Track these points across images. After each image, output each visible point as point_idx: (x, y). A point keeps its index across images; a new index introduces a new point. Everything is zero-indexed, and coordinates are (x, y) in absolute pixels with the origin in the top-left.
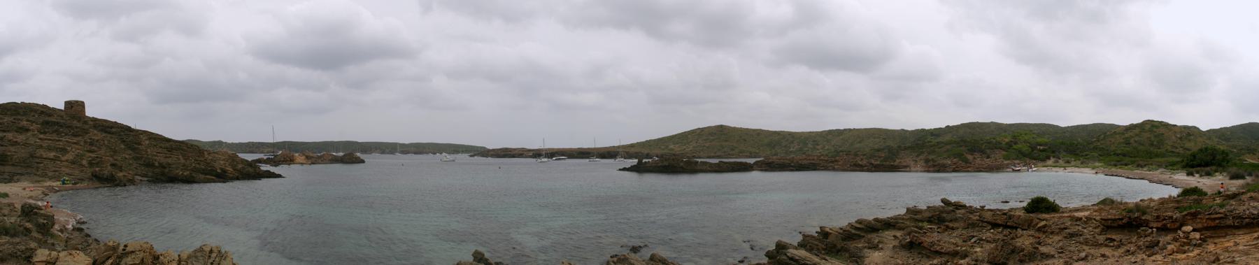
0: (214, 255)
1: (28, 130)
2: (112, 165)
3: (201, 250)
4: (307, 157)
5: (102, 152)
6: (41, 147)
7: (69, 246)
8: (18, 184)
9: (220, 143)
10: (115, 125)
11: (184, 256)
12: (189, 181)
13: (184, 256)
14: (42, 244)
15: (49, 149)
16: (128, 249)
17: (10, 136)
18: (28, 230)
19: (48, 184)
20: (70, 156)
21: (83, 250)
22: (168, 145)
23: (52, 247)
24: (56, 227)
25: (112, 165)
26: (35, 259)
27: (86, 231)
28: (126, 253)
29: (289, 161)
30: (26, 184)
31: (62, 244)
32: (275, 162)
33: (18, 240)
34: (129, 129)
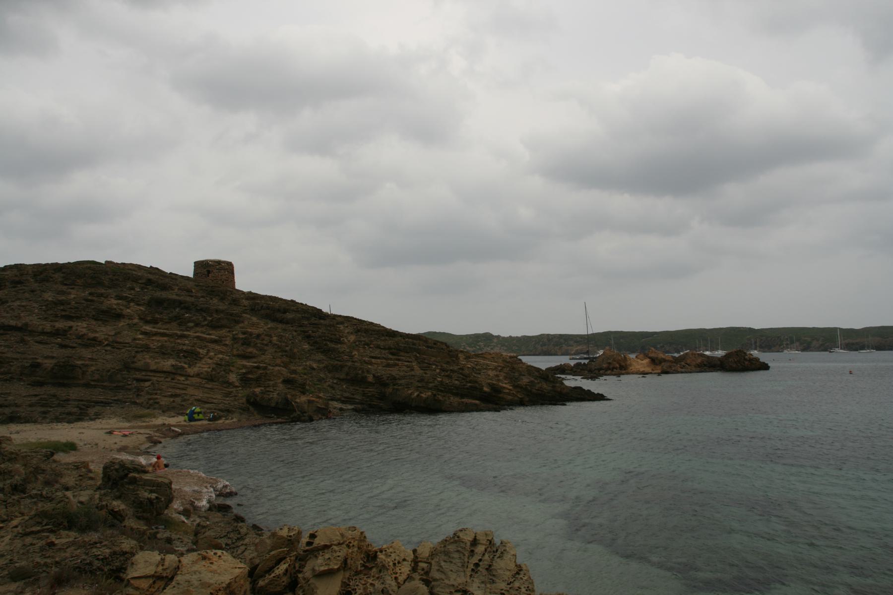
0: (480, 549)
1: (119, 316)
2: (287, 381)
3: (456, 539)
4: (654, 361)
5: (267, 357)
6: (146, 348)
7: (200, 541)
8: (97, 424)
9: (487, 338)
10: (292, 306)
11: (424, 552)
12: (431, 408)
13: (424, 552)
14: (146, 541)
15: (163, 352)
16: (318, 542)
17: (81, 327)
18: (117, 516)
19: (159, 421)
20: (203, 367)
21: (229, 548)
22: (390, 342)
23: (167, 546)
24: (177, 505)
25: (287, 381)
26: (131, 573)
27: (236, 511)
28: (313, 551)
29: (619, 368)
30: (113, 422)
31: (188, 539)
32: (592, 371)
33: (94, 536)
34: (317, 314)
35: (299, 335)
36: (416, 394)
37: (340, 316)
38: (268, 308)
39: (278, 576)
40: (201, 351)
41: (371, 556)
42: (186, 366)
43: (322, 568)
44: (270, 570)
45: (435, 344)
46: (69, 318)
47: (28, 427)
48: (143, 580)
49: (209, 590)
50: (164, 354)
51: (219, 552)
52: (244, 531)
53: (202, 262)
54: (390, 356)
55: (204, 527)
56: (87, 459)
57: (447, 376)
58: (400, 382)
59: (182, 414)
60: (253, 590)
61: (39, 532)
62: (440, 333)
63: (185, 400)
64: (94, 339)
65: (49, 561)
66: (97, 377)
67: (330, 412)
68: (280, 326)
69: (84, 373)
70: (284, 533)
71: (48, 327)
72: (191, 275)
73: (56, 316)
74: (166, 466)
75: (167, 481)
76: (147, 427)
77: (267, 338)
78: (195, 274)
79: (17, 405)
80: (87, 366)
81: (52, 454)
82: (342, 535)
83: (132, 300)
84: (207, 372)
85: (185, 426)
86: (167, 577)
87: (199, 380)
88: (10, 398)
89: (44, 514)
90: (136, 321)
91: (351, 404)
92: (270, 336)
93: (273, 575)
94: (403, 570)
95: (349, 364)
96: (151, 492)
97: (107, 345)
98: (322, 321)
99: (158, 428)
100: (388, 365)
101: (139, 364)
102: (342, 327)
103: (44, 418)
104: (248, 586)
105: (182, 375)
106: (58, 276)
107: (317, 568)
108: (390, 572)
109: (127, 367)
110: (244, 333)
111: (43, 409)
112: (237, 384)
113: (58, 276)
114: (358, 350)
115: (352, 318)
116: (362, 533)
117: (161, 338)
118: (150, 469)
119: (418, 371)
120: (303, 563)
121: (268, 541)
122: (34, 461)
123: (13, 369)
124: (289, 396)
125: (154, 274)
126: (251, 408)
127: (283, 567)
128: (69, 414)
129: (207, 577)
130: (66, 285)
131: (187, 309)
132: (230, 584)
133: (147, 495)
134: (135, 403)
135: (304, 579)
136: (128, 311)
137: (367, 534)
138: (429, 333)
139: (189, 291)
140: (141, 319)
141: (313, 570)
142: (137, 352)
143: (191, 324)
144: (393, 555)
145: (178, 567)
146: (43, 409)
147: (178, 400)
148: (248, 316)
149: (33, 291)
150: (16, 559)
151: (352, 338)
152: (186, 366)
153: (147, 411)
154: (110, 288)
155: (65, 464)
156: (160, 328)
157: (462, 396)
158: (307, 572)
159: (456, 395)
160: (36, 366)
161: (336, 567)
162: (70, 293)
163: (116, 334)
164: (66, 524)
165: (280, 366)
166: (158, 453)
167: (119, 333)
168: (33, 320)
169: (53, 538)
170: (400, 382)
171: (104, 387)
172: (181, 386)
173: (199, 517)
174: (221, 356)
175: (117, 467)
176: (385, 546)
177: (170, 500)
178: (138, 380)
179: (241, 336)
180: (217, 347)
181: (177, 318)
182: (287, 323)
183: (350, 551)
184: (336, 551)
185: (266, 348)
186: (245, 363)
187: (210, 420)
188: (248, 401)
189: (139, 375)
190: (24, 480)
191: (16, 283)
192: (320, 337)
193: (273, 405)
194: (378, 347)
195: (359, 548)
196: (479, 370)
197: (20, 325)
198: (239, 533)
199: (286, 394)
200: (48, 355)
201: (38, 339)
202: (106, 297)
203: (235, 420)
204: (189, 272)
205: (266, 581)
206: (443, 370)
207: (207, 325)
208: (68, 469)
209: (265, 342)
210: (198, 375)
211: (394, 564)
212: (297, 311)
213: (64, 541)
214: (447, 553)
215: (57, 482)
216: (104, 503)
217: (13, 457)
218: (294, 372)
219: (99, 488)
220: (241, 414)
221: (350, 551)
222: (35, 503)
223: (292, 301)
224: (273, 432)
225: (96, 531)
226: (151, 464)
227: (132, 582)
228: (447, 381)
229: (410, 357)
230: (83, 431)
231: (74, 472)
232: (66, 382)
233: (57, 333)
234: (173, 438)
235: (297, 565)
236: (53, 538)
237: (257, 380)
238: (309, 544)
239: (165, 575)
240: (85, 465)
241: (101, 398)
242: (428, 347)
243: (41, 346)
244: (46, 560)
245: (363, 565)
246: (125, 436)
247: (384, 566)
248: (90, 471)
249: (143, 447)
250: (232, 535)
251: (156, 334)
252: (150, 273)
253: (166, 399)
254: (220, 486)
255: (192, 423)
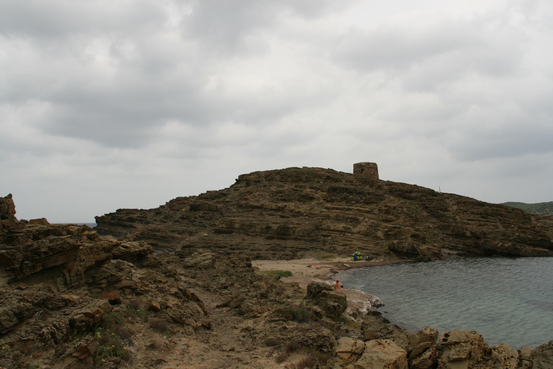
1: (312, 199)
2: (413, 236)
5: (401, 221)
6: (328, 217)
8: (302, 261)
10: (414, 188)
11: (527, 353)
12: (513, 254)
13: (527, 353)
15: (338, 219)
16: (450, 339)
17: (291, 205)
19: (337, 260)
22: (481, 210)
24: (349, 310)
25: (413, 236)
28: (447, 345)
33: (306, 326)
34: (431, 192)
35: (420, 206)
36: (500, 244)
37: (446, 194)
38: (400, 190)
39: (425, 359)
40: (360, 218)
41: (488, 352)
42: (351, 227)
43: (455, 357)
44: (420, 355)
45: (513, 210)
46: (285, 200)
47: (265, 262)
48: (345, 354)
49: (384, 364)
50: (338, 220)
51: (388, 341)
52: (391, 328)
53: (358, 164)
54: (482, 219)
55: (366, 325)
56: (297, 281)
57: (522, 232)
58: (489, 236)
59: (350, 256)
60: (409, 365)
61: (277, 321)
62: (516, 203)
63: (351, 248)
64: (299, 212)
65: (284, 337)
66: (301, 234)
67: (442, 255)
68: (408, 201)
69: (294, 232)
70: (428, 332)
71: (274, 206)
72: (352, 172)
73: (278, 200)
74: (342, 287)
75: (343, 296)
76: (330, 264)
77: (400, 209)
78: (354, 171)
79: (259, 250)
80: (295, 227)
81: (279, 278)
82: (467, 336)
83: (319, 189)
84: (364, 231)
85: (352, 263)
86: (358, 353)
87: (359, 236)
88: (256, 246)
89: (280, 311)
90: (321, 201)
91: (456, 250)
92: (402, 208)
93: (422, 358)
94: (511, 364)
95: (454, 224)
96: (335, 302)
97: (306, 216)
98: (435, 197)
99: (337, 264)
100: (480, 225)
101: (324, 227)
102: (448, 201)
103: (274, 257)
104: (406, 363)
105: (349, 233)
106: (278, 177)
107: (451, 356)
108: (502, 364)
109: (318, 228)
110: (386, 206)
111: (273, 252)
112: (382, 238)
113: (278, 177)
114: (459, 216)
115: (455, 195)
116: (481, 336)
117: (336, 211)
118: (333, 288)
119: (501, 229)
120: (441, 352)
121: (417, 336)
122: (271, 281)
123: (257, 230)
124: (415, 245)
125: (331, 173)
126: (391, 253)
127: (428, 354)
128: (287, 255)
129: (382, 356)
130: (282, 182)
131: (351, 193)
132: (396, 361)
133: (332, 303)
134: (323, 249)
135: (442, 362)
136: (317, 195)
137: (483, 336)
138: (508, 203)
139: (351, 182)
140: (324, 200)
141: (449, 357)
142: (323, 219)
143: (354, 202)
144: (504, 353)
145: (364, 348)
146: (273, 252)
147: (347, 247)
148: (388, 196)
149: (265, 186)
150: (268, 334)
151: (455, 208)
152: (351, 227)
153: (330, 254)
154: (306, 182)
155: (286, 283)
156: (335, 205)
157: (535, 246)
158: (444, 357)
159: (530, 245)
160: (268, 228)
161: (464, 357)
162: (284, 186)
163: (311, 209)
164: (291, 317)
165: (408, 226)
166: (336, 280)
167: (312, 208)
168: (266, 202)
169: (285, 325)
170: (489, 236)
171: (305, 240)
172: (349, 239)
173: (362, 318)
174: (372, 221)
175: (315, 286)
176: (497, 346)
177: (345, 307)
178: (324, 236)
179: (384, 208)
180: (369, 215)
181: (345, 198)
182: (412, 199)
183: (473, 347)
184: (463, 347)
185: (399, 215)
186: (387, 225)
187: (366, 260)
188: (389, 248)
189: (324, 233)
190: (266, 291)
191: (257, 182)
192: (434, 207)
193: (405, 251)
194: (473, 213)
195: (479, 346)
196: (547, 228)
197: (259, 205)
198: (388, 330)
199: (413, 244)
200: (275, 222)
201: (269, 213)
202: (304, 188)
203: (381, 260)
204: (351, 171)
205: (418, 362)
206: (519, 228)
207: (363, 202)
208: (288, 286)
209: (399, 212)
210: (359, 233)
211: (505, 359)
212: (418, 192)
213: (292, 327)
214: (545, 356)
215: (282, 293)
216: (309, 307)
217: (260, 279)
218: (418, 230)
219: (305, 298)
220: (385, 256)
221: (473, 347)
222: (273, 304)
223: (415, 185)
224: (405, 267)
225: (307, 322)
226: (333, 286)
227: (339, 354)
228: (523, 235)
229: (495, 220)
230: (294, 265)
231: (291, 288)
232: (284, 237)
233: (278, 209)
234: (345, 270)
235: (437, 353)
236: (285, 325)
237: (395, 235)
238: (444, 340)
239: (357, 352)
240: (297, 284)
241: (304, 246)
242: (508, 212)
243: (271, 217)
244: (283, 336)
245: (482, 358)
246: (318, 268)
247: (497, 359)
248: (300, 288)
249: (328, 275)
250: (383, 331)
251: (333, 208)
252: (328, 172)
253: (340, 247)
254: (374, 300)
255: (356, 262)
